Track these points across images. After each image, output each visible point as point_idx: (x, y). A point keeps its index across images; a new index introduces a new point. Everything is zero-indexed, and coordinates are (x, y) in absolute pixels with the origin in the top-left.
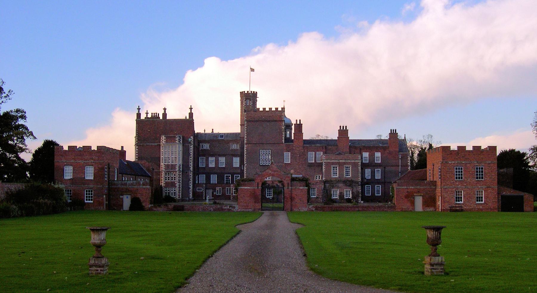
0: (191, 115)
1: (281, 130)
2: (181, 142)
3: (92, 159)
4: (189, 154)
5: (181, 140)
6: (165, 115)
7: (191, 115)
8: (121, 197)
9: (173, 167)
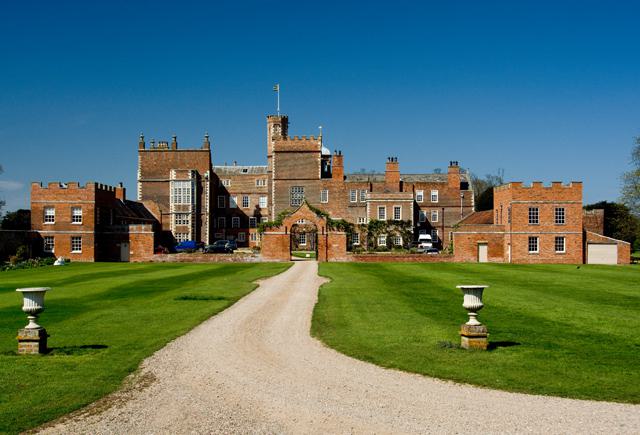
1: (317, 162)
3: (79, 198)
8: (118, 245)
9: (185, 207)
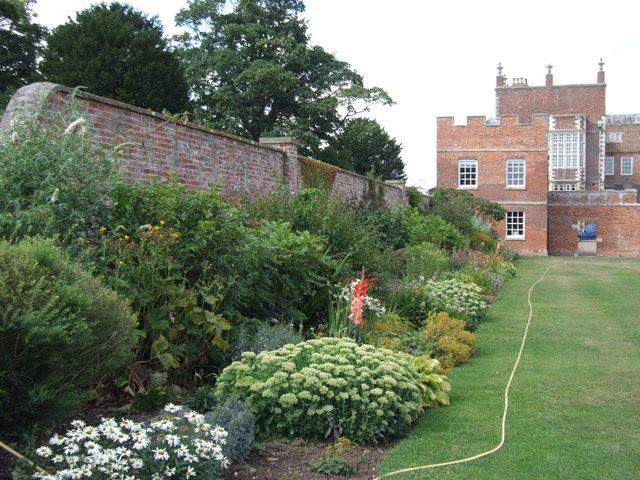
0: (601, 75)
2: (584, 126)
4: (598, 151)
5: (585, 123)
6: (549, 78)
7: (601, 75)
